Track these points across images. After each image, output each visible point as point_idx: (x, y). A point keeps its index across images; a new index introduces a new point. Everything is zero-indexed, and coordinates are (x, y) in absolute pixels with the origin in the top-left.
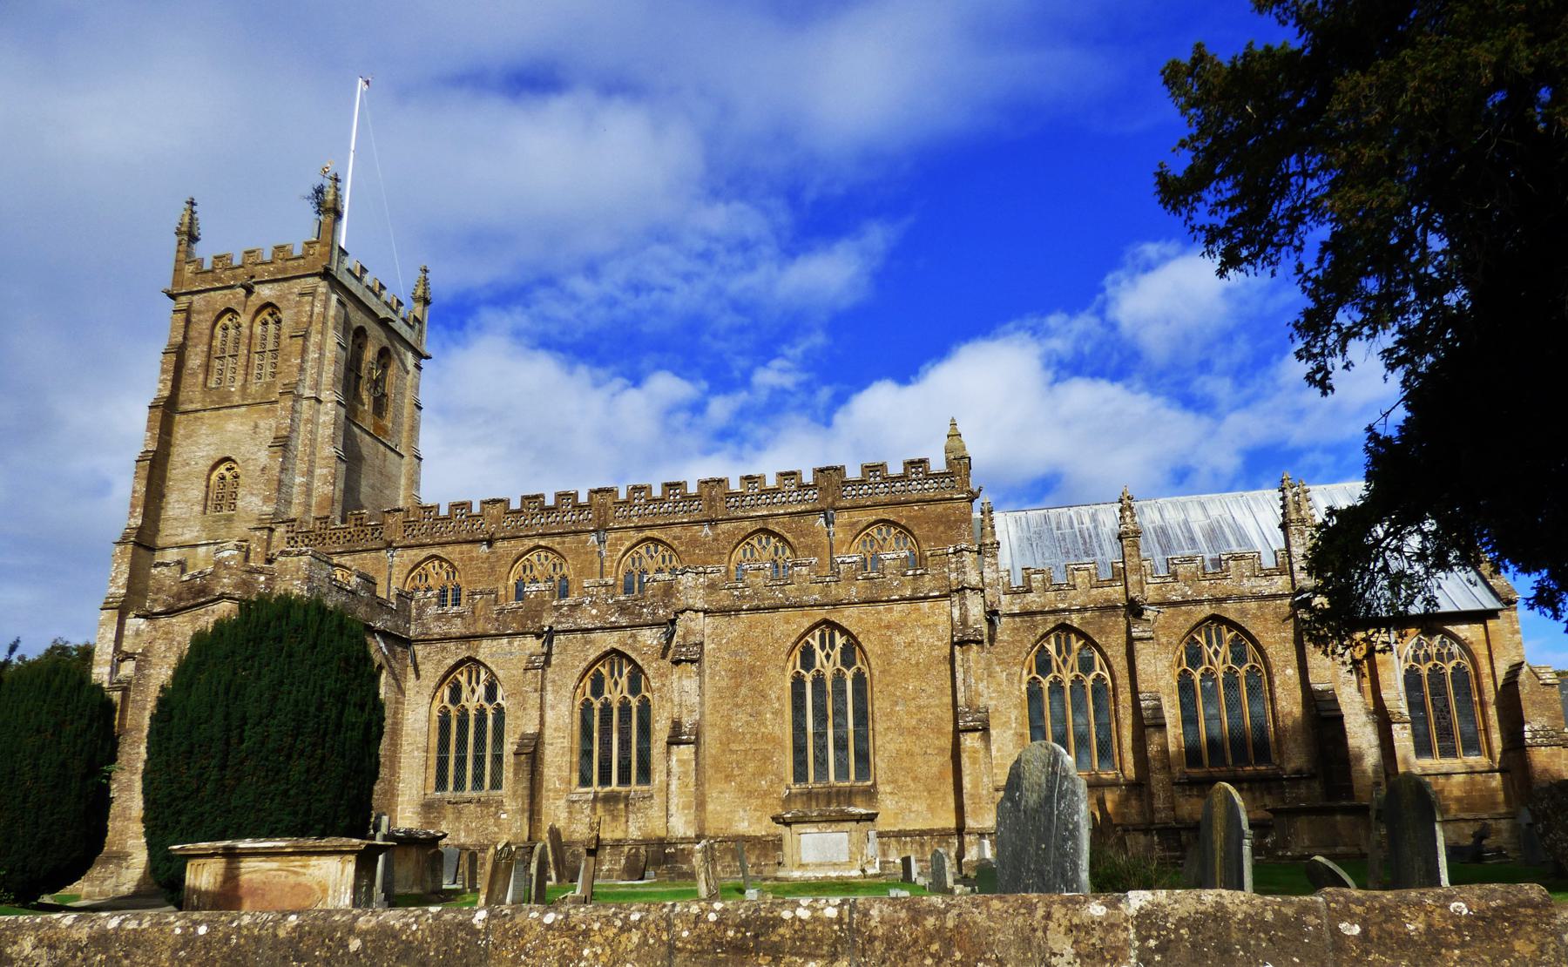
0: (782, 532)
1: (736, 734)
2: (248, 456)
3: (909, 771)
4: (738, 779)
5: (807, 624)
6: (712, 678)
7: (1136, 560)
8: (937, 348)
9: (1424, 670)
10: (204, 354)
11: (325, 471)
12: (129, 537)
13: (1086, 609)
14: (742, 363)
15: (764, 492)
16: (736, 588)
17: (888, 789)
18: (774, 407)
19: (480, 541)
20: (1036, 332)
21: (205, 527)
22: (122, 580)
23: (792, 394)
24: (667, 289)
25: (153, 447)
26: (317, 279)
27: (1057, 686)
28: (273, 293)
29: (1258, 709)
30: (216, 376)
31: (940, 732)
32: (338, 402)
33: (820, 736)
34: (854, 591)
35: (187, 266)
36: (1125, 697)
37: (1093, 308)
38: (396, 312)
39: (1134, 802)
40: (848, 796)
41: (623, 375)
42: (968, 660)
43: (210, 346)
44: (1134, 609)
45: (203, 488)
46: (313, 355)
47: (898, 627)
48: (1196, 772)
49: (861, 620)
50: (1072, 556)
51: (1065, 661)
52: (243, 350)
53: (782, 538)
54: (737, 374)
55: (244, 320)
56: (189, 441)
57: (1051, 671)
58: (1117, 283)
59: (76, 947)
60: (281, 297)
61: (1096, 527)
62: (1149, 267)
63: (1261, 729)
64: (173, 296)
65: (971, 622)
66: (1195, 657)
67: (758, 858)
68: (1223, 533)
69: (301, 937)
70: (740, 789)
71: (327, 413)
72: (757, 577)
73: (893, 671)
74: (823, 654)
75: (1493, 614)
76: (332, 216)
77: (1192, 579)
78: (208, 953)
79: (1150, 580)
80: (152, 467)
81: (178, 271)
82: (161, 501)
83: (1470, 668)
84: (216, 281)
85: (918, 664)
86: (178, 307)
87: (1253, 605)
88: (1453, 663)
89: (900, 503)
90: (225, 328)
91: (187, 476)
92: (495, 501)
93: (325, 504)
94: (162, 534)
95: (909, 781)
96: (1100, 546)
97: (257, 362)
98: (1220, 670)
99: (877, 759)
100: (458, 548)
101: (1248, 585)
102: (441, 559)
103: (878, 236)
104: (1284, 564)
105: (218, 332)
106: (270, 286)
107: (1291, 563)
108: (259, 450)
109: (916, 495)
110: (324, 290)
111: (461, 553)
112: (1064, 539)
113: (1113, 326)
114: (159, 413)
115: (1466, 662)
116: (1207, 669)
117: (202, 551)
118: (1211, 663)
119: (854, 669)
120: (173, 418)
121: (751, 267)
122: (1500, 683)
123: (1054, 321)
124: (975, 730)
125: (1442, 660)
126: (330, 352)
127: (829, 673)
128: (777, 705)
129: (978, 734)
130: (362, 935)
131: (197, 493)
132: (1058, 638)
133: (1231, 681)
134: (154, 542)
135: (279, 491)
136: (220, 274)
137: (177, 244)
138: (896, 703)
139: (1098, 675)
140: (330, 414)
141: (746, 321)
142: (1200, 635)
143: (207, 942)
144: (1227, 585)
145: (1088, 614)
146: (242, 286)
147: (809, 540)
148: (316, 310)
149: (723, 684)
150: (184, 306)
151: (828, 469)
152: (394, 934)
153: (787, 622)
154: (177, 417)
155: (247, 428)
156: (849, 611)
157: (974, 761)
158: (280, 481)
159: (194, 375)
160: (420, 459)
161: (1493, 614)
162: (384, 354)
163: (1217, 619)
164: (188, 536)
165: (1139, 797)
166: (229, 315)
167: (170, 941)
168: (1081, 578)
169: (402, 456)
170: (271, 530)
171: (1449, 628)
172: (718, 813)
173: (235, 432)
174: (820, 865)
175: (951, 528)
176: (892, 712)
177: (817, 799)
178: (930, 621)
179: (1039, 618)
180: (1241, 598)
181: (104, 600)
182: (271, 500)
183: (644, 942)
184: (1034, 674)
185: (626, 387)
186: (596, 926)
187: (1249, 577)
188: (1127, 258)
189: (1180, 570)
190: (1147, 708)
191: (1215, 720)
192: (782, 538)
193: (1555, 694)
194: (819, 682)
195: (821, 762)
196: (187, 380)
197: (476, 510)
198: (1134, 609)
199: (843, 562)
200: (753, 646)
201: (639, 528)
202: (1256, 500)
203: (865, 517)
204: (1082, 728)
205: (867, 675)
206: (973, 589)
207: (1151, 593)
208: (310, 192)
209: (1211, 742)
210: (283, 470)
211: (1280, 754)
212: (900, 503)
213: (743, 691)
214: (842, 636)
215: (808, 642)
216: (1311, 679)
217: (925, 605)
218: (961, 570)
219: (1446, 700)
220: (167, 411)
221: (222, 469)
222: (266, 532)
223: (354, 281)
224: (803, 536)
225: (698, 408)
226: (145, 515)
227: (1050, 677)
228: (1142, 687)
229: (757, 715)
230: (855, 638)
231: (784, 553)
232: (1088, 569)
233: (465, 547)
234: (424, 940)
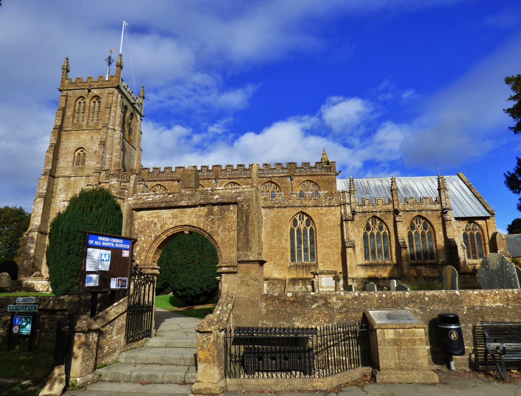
0: (276, 182)
1: (273, 246)
2: (89, 147)
3: (328, 259)
4: (274, 261)
5: (296, 213)
6: (265, 228)
7: (396, 197)
8: (268, 124)
9: (468, 233)
10: (72, 111)
11: (117, 154)
12: (47, 173)
13: (381, 212)
14: (205, 124)
15: (270, 169)
16: (273, 200)
17: (321, 265)
18: (215, 139)
19: (175, 180)
20: (299, 121)
21: (73, 171)
22: (45, 187)
23: (220, 135)
24: (181, 100)
25: (55, 142)
26: (114, 89)
27: (372, 235)
28: (98, 92)
29: (431, 244)
30: (76, 119)
31: (337, 247)
32: (121, 131)
33: (299, 247)
34: (310, 203)
35: (66, 81)
36: (393, 238)
37: (317, 115)
38: (135, 101)
39: (396, 270)
40: (309, 266)
41: (164, 126)
42: (348, 226)
43: (75, 109)
44: (396, 212)
45: (73, 157)
46: (113, 114)
47: (324, 215)
48: (413, 262)
49: (313, 212)
50: (363, 194)
51: (374, 227)
52: (87, 111)
53: (276, 184)
54: (203, 128)
55: (87, 101)
56: (67, 141)
57: (370, 230)
58: (325, 108)
59: (349, 300)
60: (101, 94)
61: (369, 185)
62: (334, 104)
63: (432, 250)
64: (61, 91)
65: (347, 214)
66: (412, 227)
67: (281, 285)
68: (407, 189)
69: (412, 297)
70: (275, 263)
71: (117, 134)
72: (280, 197)
73: (323, 228)
74: (300, 222)
75: (488, 218)
76: (120, 68)
77: (413, 204)
78: (387, 301)
79: (400, 204)
80: (55, 149)
81: (62, 82)
82: (57, 161)
83: (481, 233)
84: (77, 86)
85: (330, 226)
86: (63, 94)
87: (430, 212)
88: (476, 232)
89: (314, 175)
90: (80, 103)
91: (67, 153)
92: (180, 167)
93: (117, 165)
94: (58, 172)
95: (328, 262)
96: (371, 191)
97: (91, 115)
98: (420, 232)
99: (318, 255)
100: (167, 182)
101: (429, 207)
102: (161, 185)
103: (250, 88)
104: (439, 201)
105: (77, 104)
106: (97, 90)
107: (441, 201)
108: (93, 145)
109: (319, 173)
110: (117, 93)
111: (168, 184)
112: (360, 189)
113: (324, 121)
114: (57, 131)
115: (480, 232)
116: (416, 231)
117: (72, 179)
118: (417, 229)
119: (310, 227)
120: (61, 132)
121: (209, 94)
122: (490, 238)
123: (305, 118)
124: (351, 247)
125: (467, 231)
126: (119, 113)
127: (302, 228)
128: (286, 237)
129: (352, 248)
130: (428, 297)
131: (70, 159)
132: (372, 220)
133: (423, 235)
134: (55, 175)
135: (102, 160)
136: (77, 84)
137: (62, 72)
138: (324, 238)
139: (385, 232)
140: (118, 134)
141: (206, 111)
142: (414, 221)
143: (386, 299)
144: (423, 206)
145: (382, 213)
146: (88, 89)
147: (285, 185)
148: (114, 99)
149: (269, 230)
150: (65, 94)
151: (291, 163)
152: (437, 297)
153: (289, 212)
154: (63, 132)
155: (89, 138)
156: (309, 209)
157: (351, 257)
158: (103, 156)
159: (69, 118)
160: (142, 151)
161: (488, 218)
162: (132, 114)
163: (420, 216)
164: (67, 173)
165: (397, 269)
166: (81, 99)
167: (375, 298)
168: (380, 202)
169: (136, 149)
170: (100, 173)
171: (476, 221)
172: (267, 271)
173: (84, 139)
174: (327, 287)
175: (330, 184)
176: (323, 241)
177: (299, 267)
178: (334, 213)
179: (367, 213)
180: (427, 210)
181: (38, 195)
182: (100, 163)
183: (501, 298)
184: (365, 231)
185: (165, 130)
186: (488, 294)
187: (429, 204)
188: (327, 101)
189: (409, 201)
190: (401, 242)
191: (418, 246)
192: (276, 184)
193: (505, 242)
194: (299, 231)
195: (300, 256)
196: (66, 120)
197: (173, 170)
198: (396, 212)
199: (307, 194)
200: (278, 219)
201: (229, 179)
202: (416, 180)
203: (303, 179)
204: (379, 248)
205: (314, 229)
206: (348, 204)
207: (401, 207)
208: (107, 57)
209: (417, 253)
210: (103, 153)
211: (438, 257)
212: (314, 175)
213: (275, 233)
214: (306, 216)
215: (295, 218)
216: (448, 235)
217: (333, 208)
218: (344, 198)
219: (474, 242)
220: (59, 130)
221: (79, 151)
222: (98, 174)
223: (125, 90)
224: (283, 184)
225: (189, 138)
226: (52, 166)
227: (370, 232)
228: (399, 236)
229: (280, 240)
230: (310, 217)
231: (276, 189)
232: (382, 200)
233: (170, 182)
234: (445, 298)
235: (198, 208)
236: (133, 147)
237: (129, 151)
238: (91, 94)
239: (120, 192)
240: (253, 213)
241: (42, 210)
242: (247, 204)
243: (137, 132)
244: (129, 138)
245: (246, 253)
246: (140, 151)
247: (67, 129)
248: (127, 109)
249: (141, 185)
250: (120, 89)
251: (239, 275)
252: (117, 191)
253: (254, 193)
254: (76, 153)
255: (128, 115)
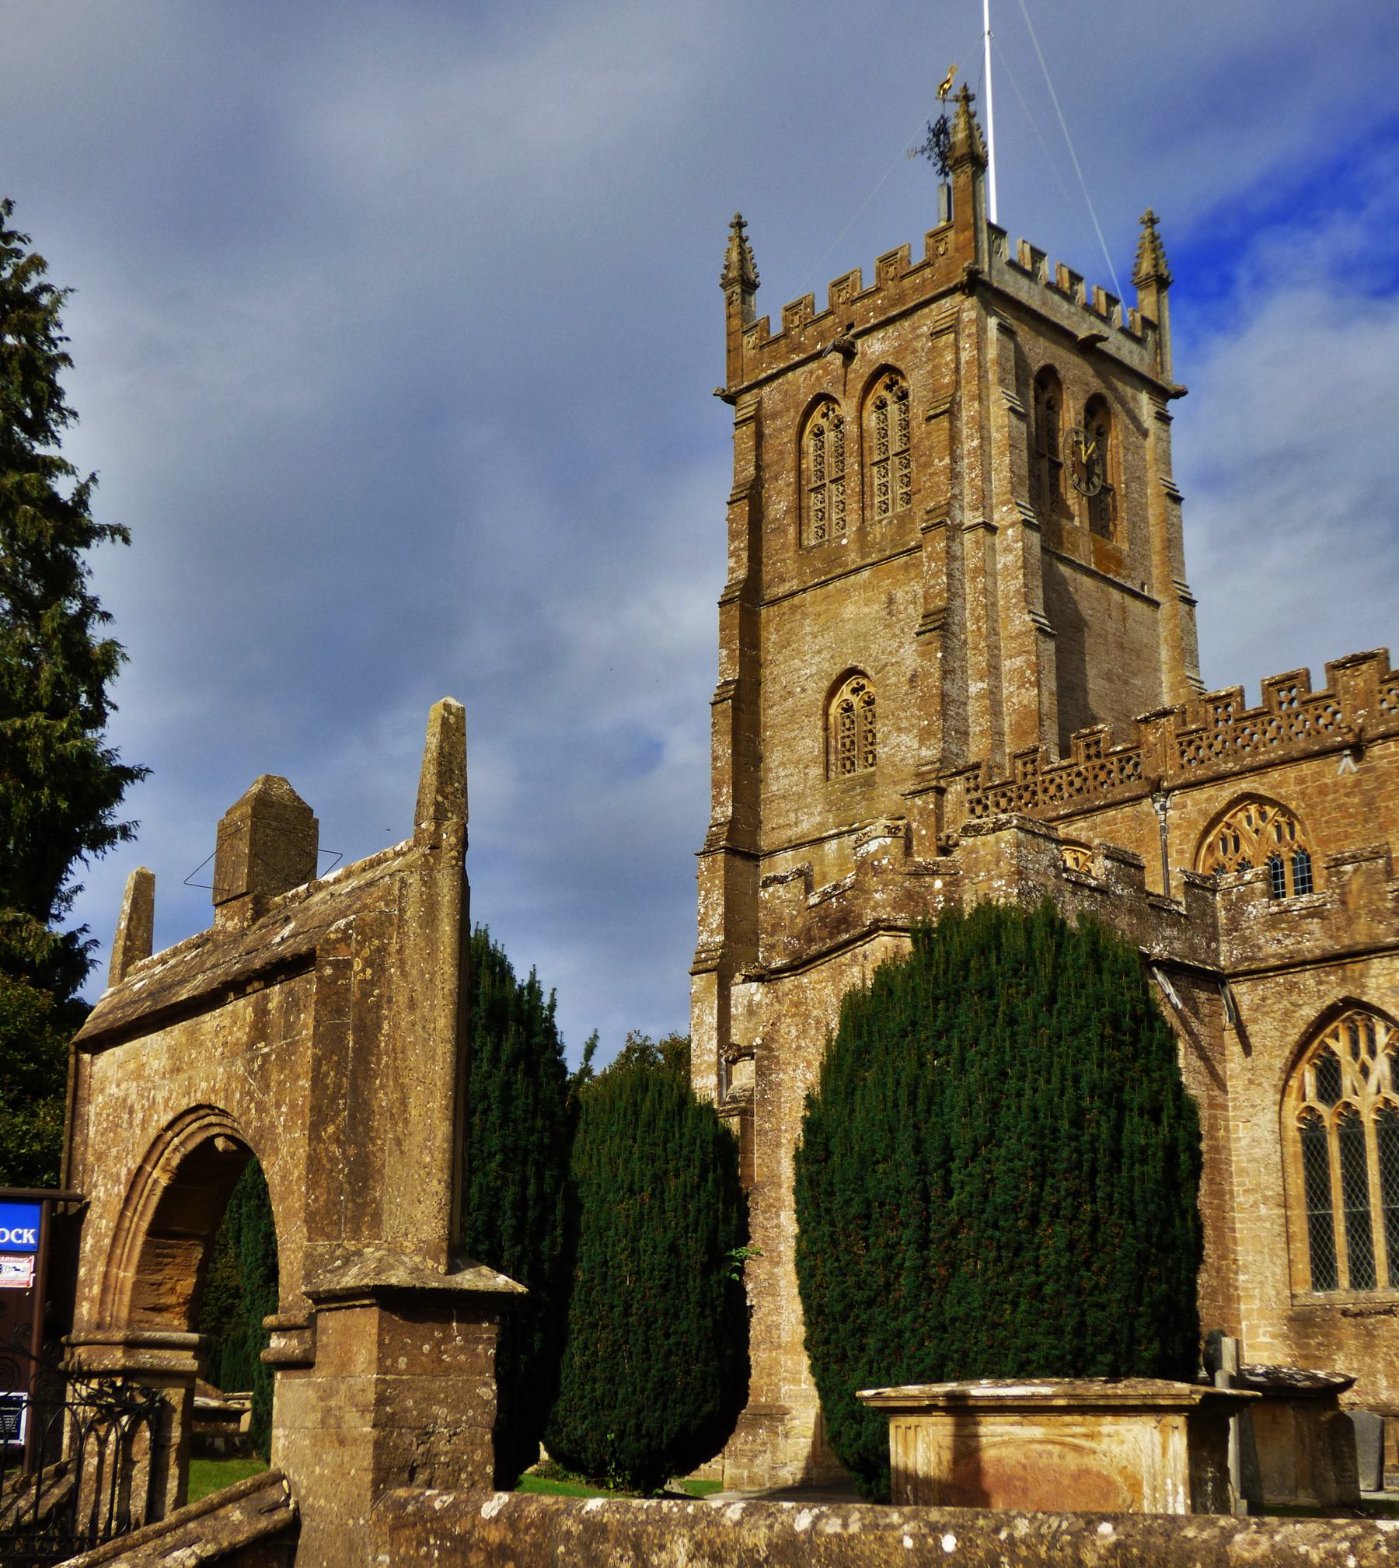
10: (791, 489)
11: (1019, 661)
19: (1337, 750)
21: (830, 803)
22: (716, 919)
26: (958, 297)
28: (886, 346)
32: (1026, 524)
35: (745, 339)
45: (819, 732)
46: (970, 444)
52: (852, 465)
71: (1008, 550)
76: (968, 169)
80: (736, 709)
82: (757, 768)
84: (793, 351)
90: (819, 433)
92: (1357, 660)
93: (1027, 725)
94: (767, 826)
97: (877, 482)
100: (1292, 772)
105: (809, 442)
106: (881, 334)
111: (1301, 781)
114: (735, 611)
117: (831, 847)
126: (999, 429)
131: (810, 744)
135: (944, 714)
137: (725, 303)
146: (836, 348)
148: (965, 356)
155: (876, 608)
158: (943, 695)
162: (1096, 408)
164: (807, 825)
166: (822, 408)
169: (1155, 604)
170: (941, 792)
173: (857, 620)
196: (772, 543)
197: (1319, 685)
208: (923, 137)
210: (946, 673)
222: (931, 797)
223: (1024, 282)
226: (736, 799)
233: (1308, 768)
235: (230, 1007)
236: (1136, 595)
237: (1111, 626)
238: (860, 369)
239: (910, 895)
240: (402, 999)
241: (715, 1034)
242: (366, 952)
243: (1151, 500)
244: (1103, 555)
245: (351, 1245)
246: (1183, 608)
247: (782, 590)
248: (1059, 384)
249: (1007, 835)
250: (987, 286)
251: (319, 1377)
252: (894, 892)
253: (414, 880)
254: (835, 709)
255: (1070, 414)
